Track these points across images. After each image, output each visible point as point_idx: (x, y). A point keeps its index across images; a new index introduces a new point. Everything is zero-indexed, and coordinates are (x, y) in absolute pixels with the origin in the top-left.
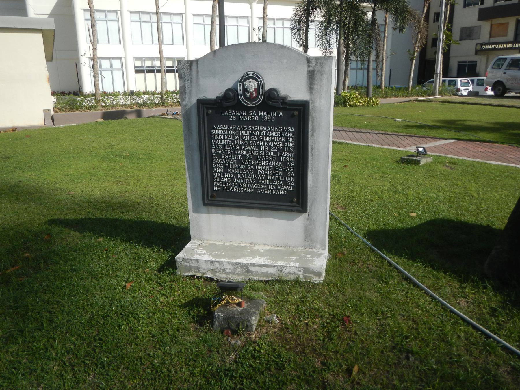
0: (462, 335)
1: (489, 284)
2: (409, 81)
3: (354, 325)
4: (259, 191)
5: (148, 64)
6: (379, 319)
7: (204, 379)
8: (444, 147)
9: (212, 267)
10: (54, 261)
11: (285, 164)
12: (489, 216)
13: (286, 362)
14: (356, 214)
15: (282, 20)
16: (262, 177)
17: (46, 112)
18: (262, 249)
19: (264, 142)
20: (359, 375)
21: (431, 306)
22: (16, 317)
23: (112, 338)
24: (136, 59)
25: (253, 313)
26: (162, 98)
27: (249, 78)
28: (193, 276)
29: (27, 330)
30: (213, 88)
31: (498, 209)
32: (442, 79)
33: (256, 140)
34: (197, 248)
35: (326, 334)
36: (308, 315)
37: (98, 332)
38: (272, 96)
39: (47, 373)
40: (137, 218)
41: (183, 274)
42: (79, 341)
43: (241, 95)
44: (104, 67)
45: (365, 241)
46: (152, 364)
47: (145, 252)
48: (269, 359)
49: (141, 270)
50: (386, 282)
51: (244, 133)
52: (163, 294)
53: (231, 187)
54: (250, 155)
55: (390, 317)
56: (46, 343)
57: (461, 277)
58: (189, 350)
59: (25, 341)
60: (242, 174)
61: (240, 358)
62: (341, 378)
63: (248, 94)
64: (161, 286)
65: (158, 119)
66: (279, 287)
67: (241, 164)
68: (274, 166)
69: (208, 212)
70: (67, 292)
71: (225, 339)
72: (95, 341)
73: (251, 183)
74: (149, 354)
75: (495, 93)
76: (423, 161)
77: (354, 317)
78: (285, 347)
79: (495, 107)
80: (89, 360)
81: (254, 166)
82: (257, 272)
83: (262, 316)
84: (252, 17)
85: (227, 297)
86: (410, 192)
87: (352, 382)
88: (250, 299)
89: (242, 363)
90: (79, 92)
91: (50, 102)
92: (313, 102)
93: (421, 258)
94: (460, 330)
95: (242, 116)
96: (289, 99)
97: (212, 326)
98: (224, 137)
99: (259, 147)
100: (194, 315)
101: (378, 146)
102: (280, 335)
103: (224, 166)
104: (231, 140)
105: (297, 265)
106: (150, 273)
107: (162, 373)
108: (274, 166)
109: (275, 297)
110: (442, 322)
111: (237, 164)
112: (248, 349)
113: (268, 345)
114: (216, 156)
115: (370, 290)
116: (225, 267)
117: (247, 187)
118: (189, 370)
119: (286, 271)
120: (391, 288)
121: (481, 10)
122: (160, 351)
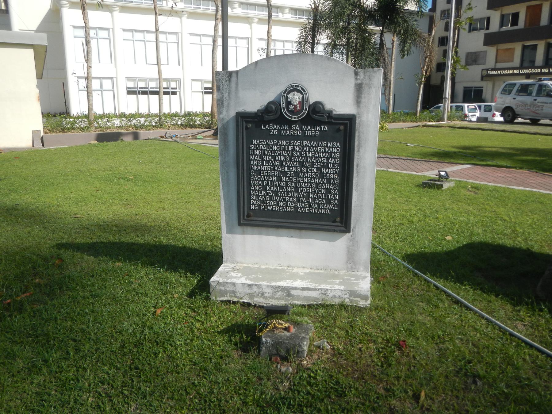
0: (527, 358)
1: (545, 307)
2: (417, 106)
3: (412, 350)
4: (299, 210)
5: (142, 84)
6: (437, 344)
7: (258, 408)
8: (462, 171)
9: (250, 291)
10: (70, 286)
11: (329, 181)
12: (526, 239)
13: (346, 389)
14: (389, 237)
15: (283, 41)
16: (303, 195)
17: (35, 133)
18: (302, 272)
19: (307, 158)
20: (427, 400)
21: (489, 329)
22: (36, 346)
23: (149, 367)
24: (129, 79)
25: (303, 338)
26: (160, 120)
27: (293, 90)
28: (229, 302)
29: (51, 359)
30: (254, 101)
31: (534, 233)
32: (450, 104)
33: (298, 156)
34: (231, 271)
35: (383, 359)
36: (360, 340)
37: (133, 361)
38: (317, 110)
39: (82, 405)
40: (156, 242)
41: (218, 299)
42: (112, 370)
43: (284, 108)
44: (105, 87)
45: (405, 264)
46: (198, 393)
47: (173, 277)
48: (327, 386)
49: (169, 296)
50: (436, 306)
51: (286, 148)
52: (198, 320)
53: (270, 205)
54: (291, 171)
55: (448, 341)
56: (76, 373)
57: (514, 300)
58: (237, 378)
59: (51, 371)
60: (281, 192)
61: (294, 385)
62: (408, 404)
63: (292, 108)
64: (195, 311)
65: (157, 142)
66: (325, 312)
67: (281, 181)
68: (317, 184)
69: (243, 233)
70: (92, 319)
71: (275, 366)
72: (131, 370)
73: (291, 202)
74: (193, 383)
75: (504, 119)
76: (446, 185)
77: (411, 341)
78: (342, 373)
79: (507, 133)
80: (128, 391)
81: (296, 183)
82: (298, 296)
83: (312, 341)
84: (251, 38)
85: (275, 321)
86: (441, 216)
87: (422, 408)
88: (296, 324)
89: (298, 391)
90: (66, 113)
91: (38, 123)
92: (360, 117)
93: (468, 281)
94: (525, 352)
95: (284, 130)
96: (334, 113)
97: (259, 353)
98: (264, 153)
99: (301, 163)
100: (236, 342)
101: (394, 171)
102: (333, 361)
103: (263, 183)
104: (272, 156)
105: (342, 288)
106: (179, 298)
107: (212, 402)
108: (317, 184)
109: (321, 322)
110: (503, 344)
111: (277, 181)
112: (302, 376)
113: (323, 372)
114: (255, 173)
115: (421, 314)
116: (264, 291)
117: (287, 206)
118: (241, 399)
119: (331, 294)
120: (443, 311)
121: (486, 35)
122: (205, 380)
